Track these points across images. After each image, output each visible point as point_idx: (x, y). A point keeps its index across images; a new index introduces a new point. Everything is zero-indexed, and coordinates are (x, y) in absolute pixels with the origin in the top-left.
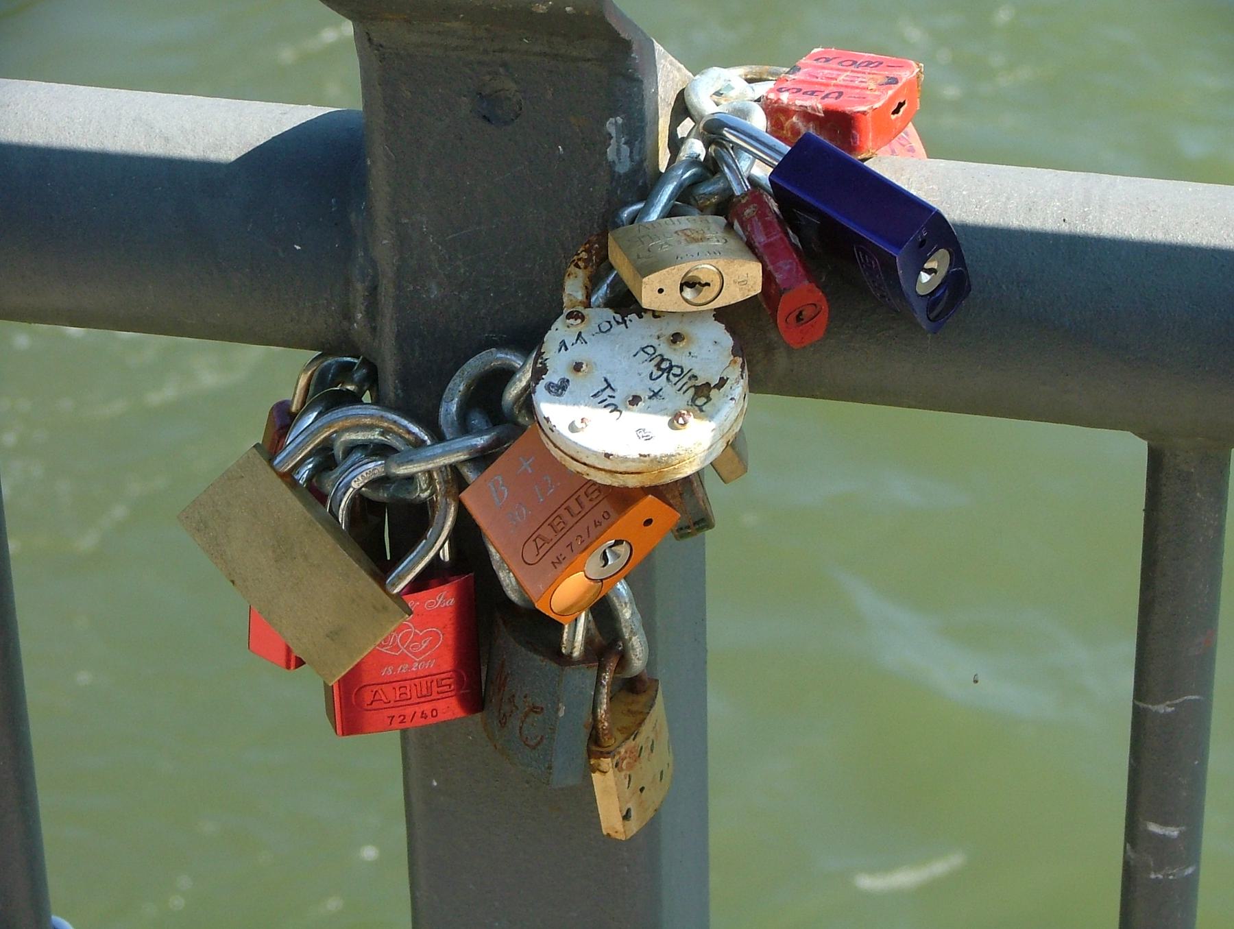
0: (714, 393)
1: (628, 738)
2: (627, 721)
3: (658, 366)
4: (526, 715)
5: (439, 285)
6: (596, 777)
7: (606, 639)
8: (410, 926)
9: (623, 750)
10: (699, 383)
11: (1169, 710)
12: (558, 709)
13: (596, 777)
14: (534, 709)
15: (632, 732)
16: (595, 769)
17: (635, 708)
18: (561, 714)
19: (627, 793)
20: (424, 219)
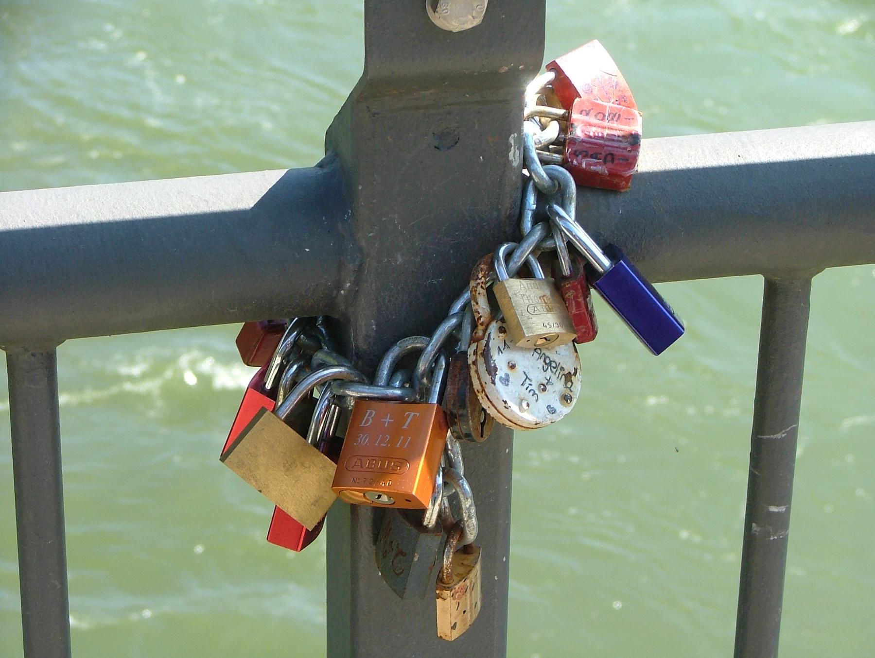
0: (573, 377)
1: (460, 581)
2: (461, 570)
3: (545, 361)
4: (396, 555)
5: (402, 255)
6: (439, 601)
7: (450, 526)
8: (870, 124)
9: (457, 587)
10: (566, 372)
11: (783, 436)
12: (414, 556)
13: (439, 601)
14: (402, 553)
15: (463, 577)
16: (438, 597)
17: (465, 562)
18: (416, 559)
19: (455, 613)
20: (396, 216)
